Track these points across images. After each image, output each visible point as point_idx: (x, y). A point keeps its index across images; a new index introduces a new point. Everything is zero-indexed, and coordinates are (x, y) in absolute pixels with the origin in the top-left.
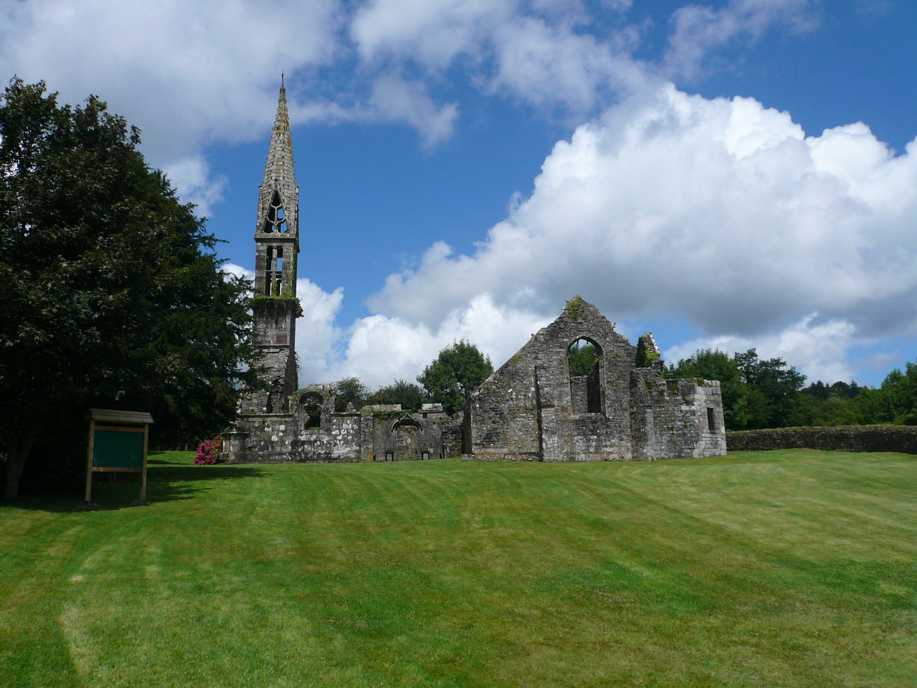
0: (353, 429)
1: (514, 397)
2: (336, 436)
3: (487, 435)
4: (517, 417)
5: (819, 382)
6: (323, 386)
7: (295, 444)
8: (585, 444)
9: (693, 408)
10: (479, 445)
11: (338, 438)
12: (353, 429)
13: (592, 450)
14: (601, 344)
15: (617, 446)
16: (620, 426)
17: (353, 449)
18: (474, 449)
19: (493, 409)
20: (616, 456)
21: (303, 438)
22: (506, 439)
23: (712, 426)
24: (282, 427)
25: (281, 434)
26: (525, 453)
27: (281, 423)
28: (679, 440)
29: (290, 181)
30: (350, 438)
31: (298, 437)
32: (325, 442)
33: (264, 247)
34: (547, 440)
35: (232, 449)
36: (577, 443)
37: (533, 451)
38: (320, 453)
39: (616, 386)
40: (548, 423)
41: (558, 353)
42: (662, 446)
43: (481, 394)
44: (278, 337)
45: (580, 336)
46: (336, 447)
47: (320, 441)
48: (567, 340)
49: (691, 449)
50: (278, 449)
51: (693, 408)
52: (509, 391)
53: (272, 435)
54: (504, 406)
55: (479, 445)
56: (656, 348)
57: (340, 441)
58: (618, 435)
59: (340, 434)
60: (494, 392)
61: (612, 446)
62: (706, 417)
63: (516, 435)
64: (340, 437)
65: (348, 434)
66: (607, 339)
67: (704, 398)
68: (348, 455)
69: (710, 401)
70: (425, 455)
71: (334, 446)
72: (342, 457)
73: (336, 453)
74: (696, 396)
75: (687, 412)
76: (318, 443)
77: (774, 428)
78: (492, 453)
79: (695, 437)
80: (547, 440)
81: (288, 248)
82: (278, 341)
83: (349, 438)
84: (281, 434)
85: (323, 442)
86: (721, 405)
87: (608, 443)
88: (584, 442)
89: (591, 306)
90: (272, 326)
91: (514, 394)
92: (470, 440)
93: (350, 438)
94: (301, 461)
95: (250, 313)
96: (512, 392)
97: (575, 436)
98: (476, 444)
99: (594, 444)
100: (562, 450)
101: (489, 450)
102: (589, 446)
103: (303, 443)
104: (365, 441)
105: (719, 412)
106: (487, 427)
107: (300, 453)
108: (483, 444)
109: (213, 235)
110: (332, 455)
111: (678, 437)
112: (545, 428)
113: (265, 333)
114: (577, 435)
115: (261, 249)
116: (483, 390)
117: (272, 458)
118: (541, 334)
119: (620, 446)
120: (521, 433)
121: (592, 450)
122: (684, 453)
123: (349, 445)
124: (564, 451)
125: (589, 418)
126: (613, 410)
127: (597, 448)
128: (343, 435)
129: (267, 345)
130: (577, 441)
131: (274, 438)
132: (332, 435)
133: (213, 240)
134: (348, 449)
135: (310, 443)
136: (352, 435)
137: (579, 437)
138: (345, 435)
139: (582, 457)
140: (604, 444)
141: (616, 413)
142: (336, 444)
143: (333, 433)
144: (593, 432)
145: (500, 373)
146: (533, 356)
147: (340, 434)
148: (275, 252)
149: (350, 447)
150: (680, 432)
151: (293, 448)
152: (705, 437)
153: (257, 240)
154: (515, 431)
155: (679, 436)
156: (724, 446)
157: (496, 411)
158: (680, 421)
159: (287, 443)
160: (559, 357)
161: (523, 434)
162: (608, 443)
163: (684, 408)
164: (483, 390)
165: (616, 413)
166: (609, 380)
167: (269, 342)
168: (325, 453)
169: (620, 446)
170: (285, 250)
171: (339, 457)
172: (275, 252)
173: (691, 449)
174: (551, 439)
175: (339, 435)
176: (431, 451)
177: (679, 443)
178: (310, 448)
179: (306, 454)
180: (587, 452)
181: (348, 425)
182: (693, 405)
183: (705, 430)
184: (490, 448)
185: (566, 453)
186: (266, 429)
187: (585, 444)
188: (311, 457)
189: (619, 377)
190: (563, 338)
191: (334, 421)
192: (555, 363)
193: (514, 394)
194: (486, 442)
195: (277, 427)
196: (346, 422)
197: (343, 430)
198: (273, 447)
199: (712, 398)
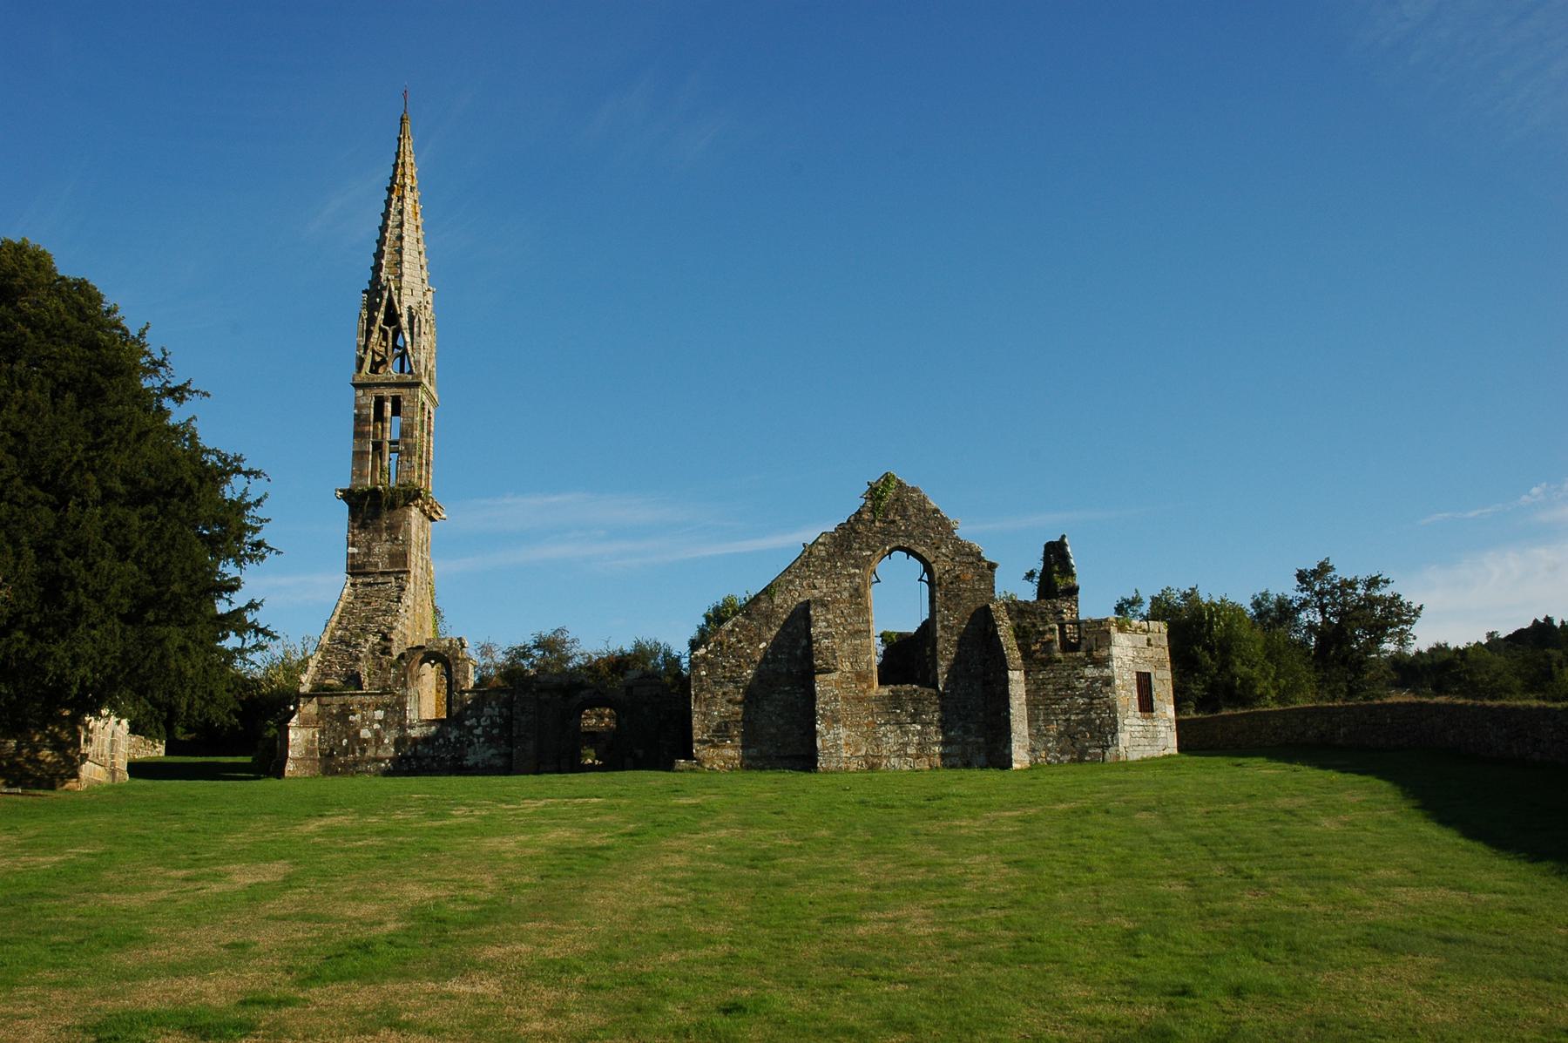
0: (501, 716)
2: (472, 728)
4: (774, 692)
5: (1548, 619)
12: (501, 716)
13: (911, 750)
14: (931, 560)
15: (959, 743)
16: (965, 707)
17: (502, 751)
24: (379, 714)
25: (376, 726)
28: (1081, 731)
30: (495, 731)
31: (406, 731)
32: (453, 740)
34: (825, 732)
36: (884, 739)
40: (826, 703)
42: (1049, 742)
43: (710, 652)
45: (893, 545)
47: (443, 737)
49: (1102, 747)
50: (370, 753)
57: (478, 737)
59: (479, 725)
64: (478, 731)
65: (493, 725)
67: (1131, 653)
68: (491, 762)
71: (469, 746)
72: (480, 765)
75: (1095, 680)
76: (441, 741)
77: (1421, 704)
79: (1109, 726)
80: (825, 732)
84: (376, 726)
85: (449, 739)
86: (1168, 665)
89: (914, 490)
90: (381, 537)
92: (692, 737)
93: (495, 731)
97: (881, 725)
99: (916, 739)
100: (858, 750)
102: (906, 745)
106: (719, 712)
108: (712, 741)
109: (189, 382)
110: (465, 762)
112: (821, 712)
113: (369, 549)
114: (885, 724)
115: (362, 402)
116: (712, 645)
117: (360, 768)
118: (821, 544)
120: (781, 722)
121: (911, 750)
122: (1090, 755)
124: (859, 754)
125: (906, 692)
129: (373, 569)
130: (885, 735)
131: (365, 733)
132: (465, 726)
133: (189, 391)
134: (492, 751)
137: (888, 727)
138: (487, 726)
142: (471, 744)
147: (479, 725)
148: (388, 406)
150: (1081, 716)
152: (1131, 726)
153: (357, 386)
155: (1079, 723)
158: (1081, 696)
159: (386, 741)
163: (1090, 672)
167: (376, 565)
168: (453, 757)
172: (388, 406)
173: (1102, 747)
175: (477, 728)
176: (640, 753)
178: (426, 750)
181: (493, 708)
184: (724, 747)
185: (865, 757)
194: (718, 737)
195: (370, 713)
196: (490, 704)
197: (484, 719)
198: (363, 750)
199: (1148, 653)
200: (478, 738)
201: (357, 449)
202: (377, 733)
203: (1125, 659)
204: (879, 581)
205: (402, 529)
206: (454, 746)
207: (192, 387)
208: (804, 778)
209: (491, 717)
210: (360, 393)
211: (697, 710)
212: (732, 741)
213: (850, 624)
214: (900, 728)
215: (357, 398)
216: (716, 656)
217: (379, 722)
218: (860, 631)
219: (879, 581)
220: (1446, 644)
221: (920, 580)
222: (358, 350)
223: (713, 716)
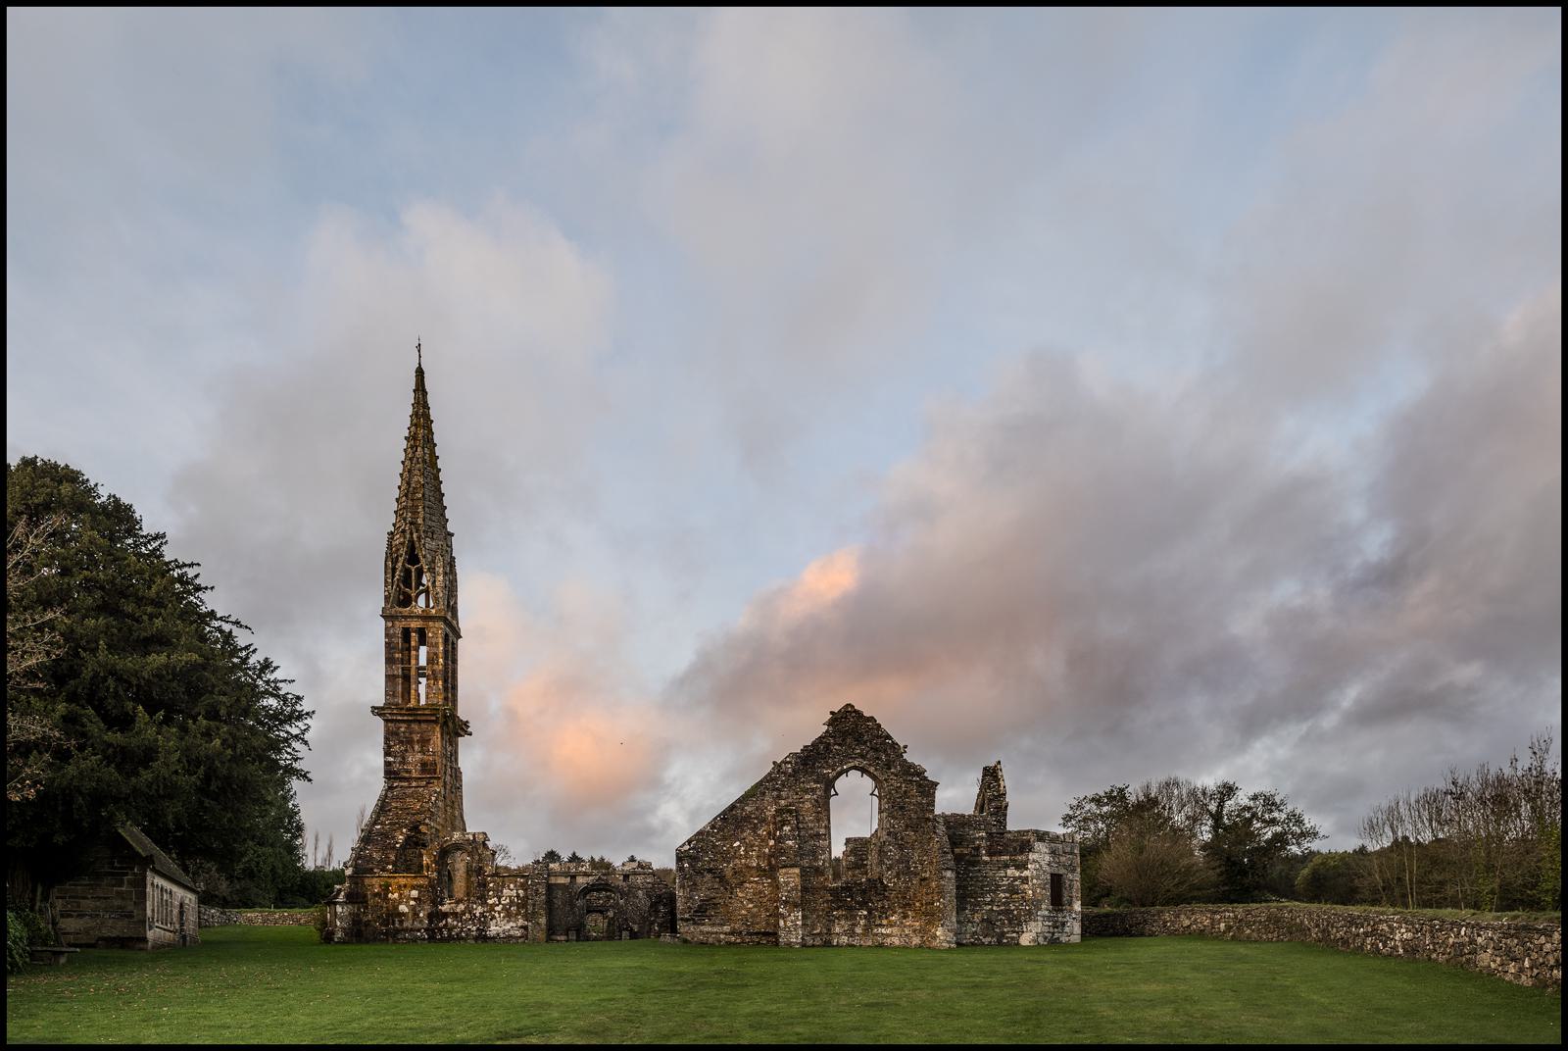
0: (518, 896)
6: (474, 835)
7: (436, 916)
9: (1026, 873)
10: (687, 920)
11: (497, 908)
13: (859, 930)
19: (710, 871)
20: (896, 941)
21: (445, 908)
22: (728, 912)
23: (1057, 900)
24: (415, 893)
25: (412, 903)
26: (757, 934)
27: (413, 888)
28: (1001, 919)
29: (434, 524)
32: (478, 915)
35: (338, 923)
38: (469, 929)
41: (813, 790)
44: (424, 764)
45: (850, 765)
46: (494, 921)
49: (1018, 933)
51: (1026, 873)
53: (400, 903)
54: (728, 868)
55: (687, 920)
57: (499, 913)
58: (900, 910)
59: (500, 903)
61: (891, 925)
63: (744, 907)
65: (512, 903)
68: (512, 933)
70: (625, 934)
73: (494, 929)
74: (1032, 856)
78: (708, 933)
81: (436, 631)
82: (423, 771)
84: (412, 903)
85: (474, 915)
87: (885, 922)
94: (443, 940)
95: (1106, 800)
96: (739, 846)
98: (682, 919)
99: (862, 922)
100: (813, 929)
103: (445, 915)
104: (534, 913)
105: (1074, 879)
106: (699, 896)
107: (440, 929)
111: (999, 914)
113: (404, 758)
114: (837, 910)
118: (790, 762)
119: (902, 926)
120: (751, 906)
121: (859, 930)
123: (513, 919)
127: (867, 929)
131: (403, 908)
132: (488, 904)
134: (512, 924)
135: (455, 915)
136: (518, 905)
140: (877, 922)
141: (899, 879)
142: (493, 918)
143: (490, 902)
144: (863, 905)
149: (514, 922)
151: (431, 922)
154: (742, 902)
156: (1077, 929)
157: (715, 873)
158: (1004, 891)
159: (421, 915)
161: (754, 907)
162: (885, 922)
163: (1011, 872)
165: (899, 879)
166: (892, 830)
168: (478, 929)
169: (902, 926)
170: (430, 635)
171: (498, 934)
173: (1018, 933)
177: (999, 923)
179: (450, 930)
180: (851, 933)
184: (703, 924)
188: (457, 934)
189: (907, 826)
190: (822, 767)
191: (491, 885)
192: (808, 805)
196: (509, 886)
202: (413, 908)
203: (1042, 863)
204: (837, 794)
205: (432, 742)
209: (510, 897)
212: (710, 920)
213: (812, 829)
216: (698, 852)
217: (414, 899)
219: (837, 794)
221: (872, 794)
223: (694, 900)
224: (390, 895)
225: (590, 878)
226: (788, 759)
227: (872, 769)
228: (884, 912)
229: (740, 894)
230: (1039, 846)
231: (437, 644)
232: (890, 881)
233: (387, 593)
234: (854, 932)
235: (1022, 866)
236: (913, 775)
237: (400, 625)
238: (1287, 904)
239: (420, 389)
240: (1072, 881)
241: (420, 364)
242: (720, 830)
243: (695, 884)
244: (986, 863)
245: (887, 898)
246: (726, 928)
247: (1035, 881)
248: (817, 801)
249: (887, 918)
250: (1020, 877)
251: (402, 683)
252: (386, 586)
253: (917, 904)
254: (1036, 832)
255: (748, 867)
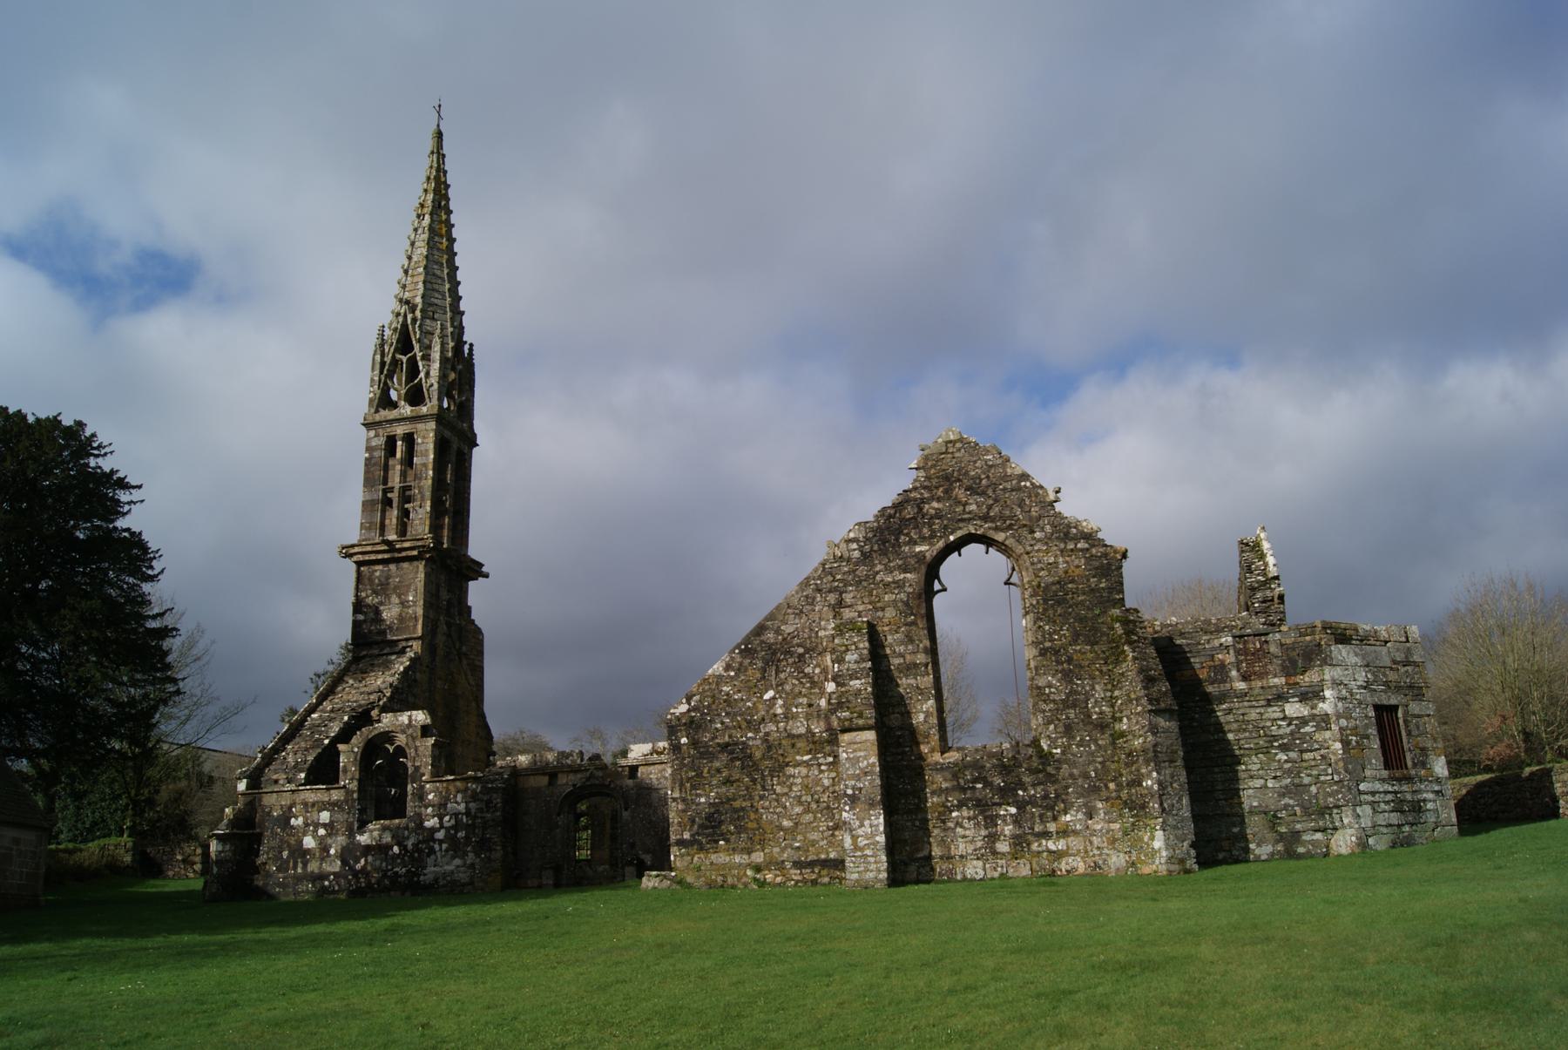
0: (468, 813)
1: (779, 711)
3: (709, 817)
8: (984, 832)
13: (1003, 847)
18: (675, 854)
24: (325, 816)
25: (322, 832)
26: (811, 864)
27: (323, 806)
28: (1286, 807)
30: (461, 834)
32: (410, 847)
33: (380, 441)
36: (959, 830)
37: (832, 855)
39: (1070, 660)
41: (899, 585)
43: (695, 709)
45: (959, 533)
46: (433, 857)
48: (924, 548)
49: (1323, 830)
52: (767, 697)
53: (305, 834)
56: (1271, 560)
57: (441, 842)
60: (729, 701)
61: (1064, 833)
62: (1373, 731)
66: (1038, 535)
67: (1361, 677)
69: (1386, 684)
71: (429, 855)
75: (1304, 721)
83: (459, 835)
84: (322, 832)
87: (1052, 827)
88: (978, 824)
91: (780, 702)
93: (461, 834)
96: (774, 698)
99: (1008, 830)
101: (713, 857)
108: (700, 843)
110: (422, 878)
111: (1283, 795)
116: (697, 698)
121: (1003, 847)
126: (1061, 729)
127: (1020, 844)
128: (448, 829)
130: (958, 824)
131: (309, 842)
134: (457, 862)
136: (467, 826)
139: (974, 869)
145: (741, 651)
146: (832, 598)
149: (462, 858)
151: (344, 862)
159: (332, 851)
160: (903, 596)
162: (1052, 827)
163: (1294, 709)
164: (697, 698)
166: (1048, 644)
170: (420, 441)
174: (867, 823)
175: (438, 830)
182: (1324, 699)
183: (1368, 773)
186: (293, 821)
187: (984, 832)
190: (913, 542)
192: (890, 613)
193: (780, 702)
197: (447, 818)
200: (440, 845)
201: (368, 498)
202: (321, 841)
206: (412, 856)
207: (103, 445)
208: (1553, 823)
210: (372, 433)
211: (676, 795)
212: (727, 841)
214: (982, 812)
215: (368, 440)
216: (703, 714)
218: (916, 665)
219: (945, 590)
220: (140, 533)
221: (1007, 583)
222: (372, 386)
224: (293, 820)
225: (579, 776)
226: (852, 535)
227: (1000, 537)
228: (1052, 806)
229: (778, 789)
230: (1341, 652)
231: (427, 450)
232: (1053, 744)
233: (372, 395)
234: (995, 853)
235: (1311, 695)
236: (1076, 539)
237: (384, 432)
238: (436, 354)
239: (439, 152)
240: (1419, 716)
241: (438, 126)
242: (738, 671)
243: (699, 775)
244: (1242, 695)
245: (1052, 779)
246: (758, 857)
247: (1343, 722)
248: (906, 604)
249: (1055, 819)
250: (1313, 717)
251: (83, 459)
252: (372, 386)
253: (1112, 786)
254: (1326, 627)
255: (791, 736)
